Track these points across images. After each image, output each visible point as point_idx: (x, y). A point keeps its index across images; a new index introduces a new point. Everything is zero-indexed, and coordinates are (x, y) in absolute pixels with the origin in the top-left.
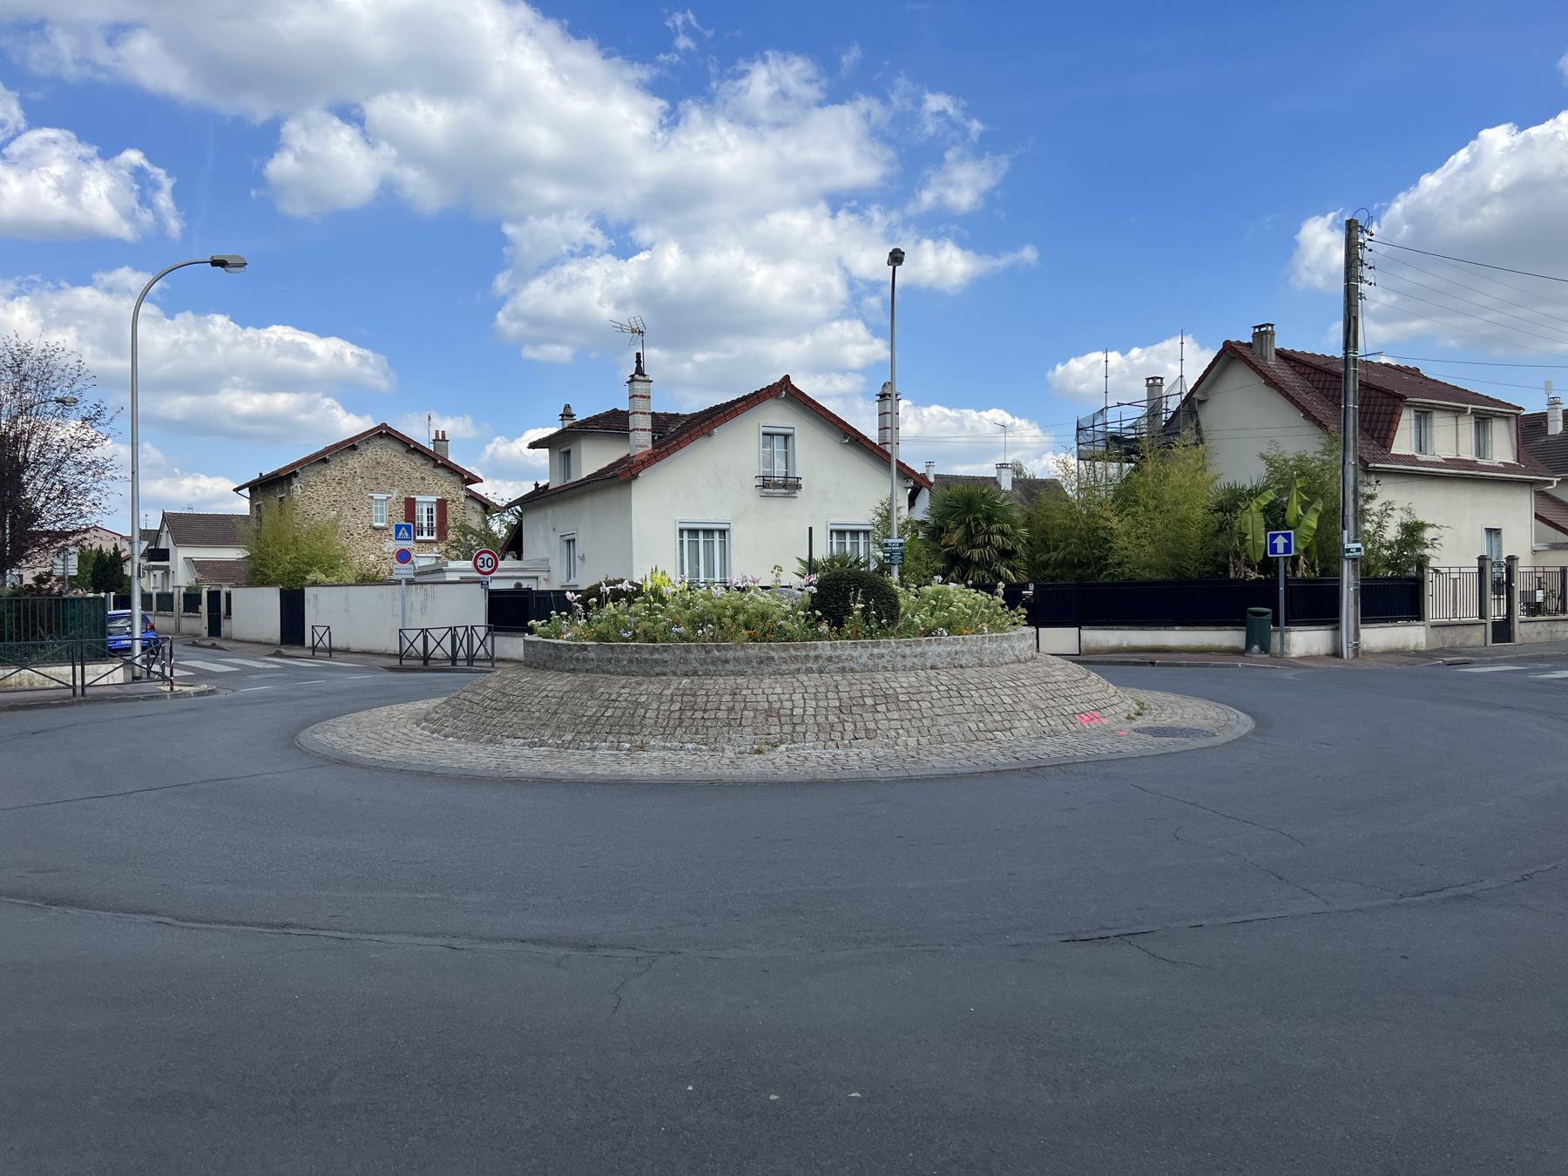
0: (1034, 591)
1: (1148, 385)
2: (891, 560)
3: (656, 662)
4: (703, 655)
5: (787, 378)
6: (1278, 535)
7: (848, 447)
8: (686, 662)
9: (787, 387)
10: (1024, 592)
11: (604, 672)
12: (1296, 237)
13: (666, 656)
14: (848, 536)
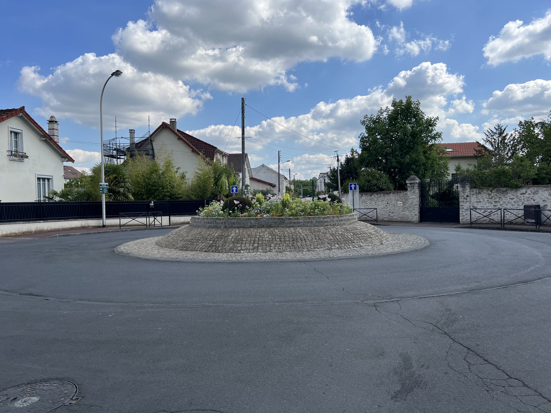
0: (154, 203)
1: (130, 132)
2: (103, 191)
3: (325, 221)
4: (337, 219)
5: (24, 107)
6: (234, 187)
7: (43, 142)
8: (333, 221)
9: (23, 112)
10: (150, 204)
11: (306, 226)
12: (20, 72)
13: (328, 220)
14: (41, 180)
